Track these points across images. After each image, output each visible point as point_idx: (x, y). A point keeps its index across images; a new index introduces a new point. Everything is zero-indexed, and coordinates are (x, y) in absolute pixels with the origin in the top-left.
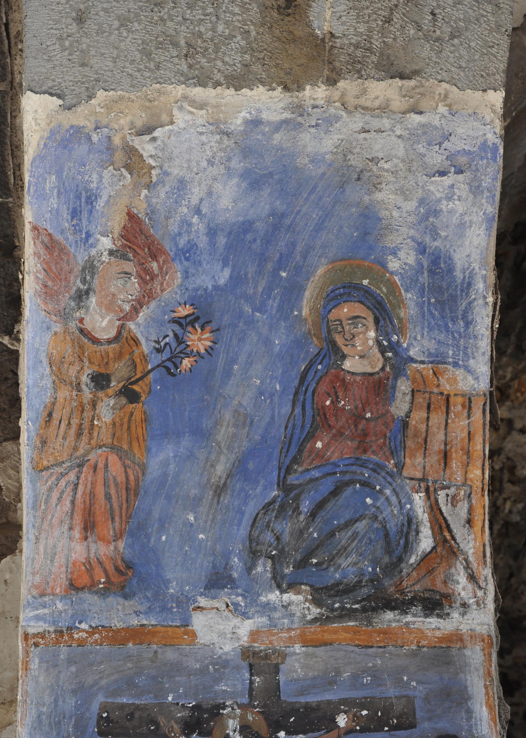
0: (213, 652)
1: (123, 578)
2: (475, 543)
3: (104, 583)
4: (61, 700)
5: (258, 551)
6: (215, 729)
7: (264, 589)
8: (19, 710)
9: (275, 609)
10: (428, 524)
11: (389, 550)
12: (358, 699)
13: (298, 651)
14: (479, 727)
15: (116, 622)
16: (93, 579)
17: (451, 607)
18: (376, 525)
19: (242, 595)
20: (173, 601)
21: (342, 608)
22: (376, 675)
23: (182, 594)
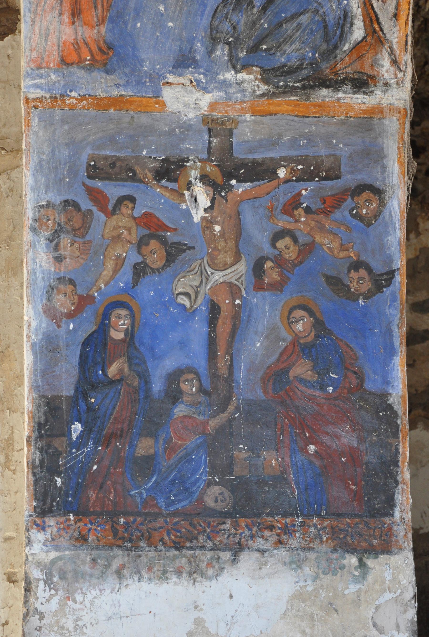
0: (179, 118)
1: (105, 57)
2: (400, 33)
3: (89, 60)
4: (57, 150)
5: (218, 38)
6: (180, 177)
7: (222, 70)
8: (24, 156)
9: (230, 85)
10: (361, 18)
11: (327, 39)
12: (295, 157)
13: (248, 119)
14: (391, 178)
15: (100, 92)
16: (80, 57)
17: (375, 86)
18: (317, 18)
19: (203, 74)
20: (146, 77)
21: (286, 86)
22: (311, 139)
23: (154, 72)
